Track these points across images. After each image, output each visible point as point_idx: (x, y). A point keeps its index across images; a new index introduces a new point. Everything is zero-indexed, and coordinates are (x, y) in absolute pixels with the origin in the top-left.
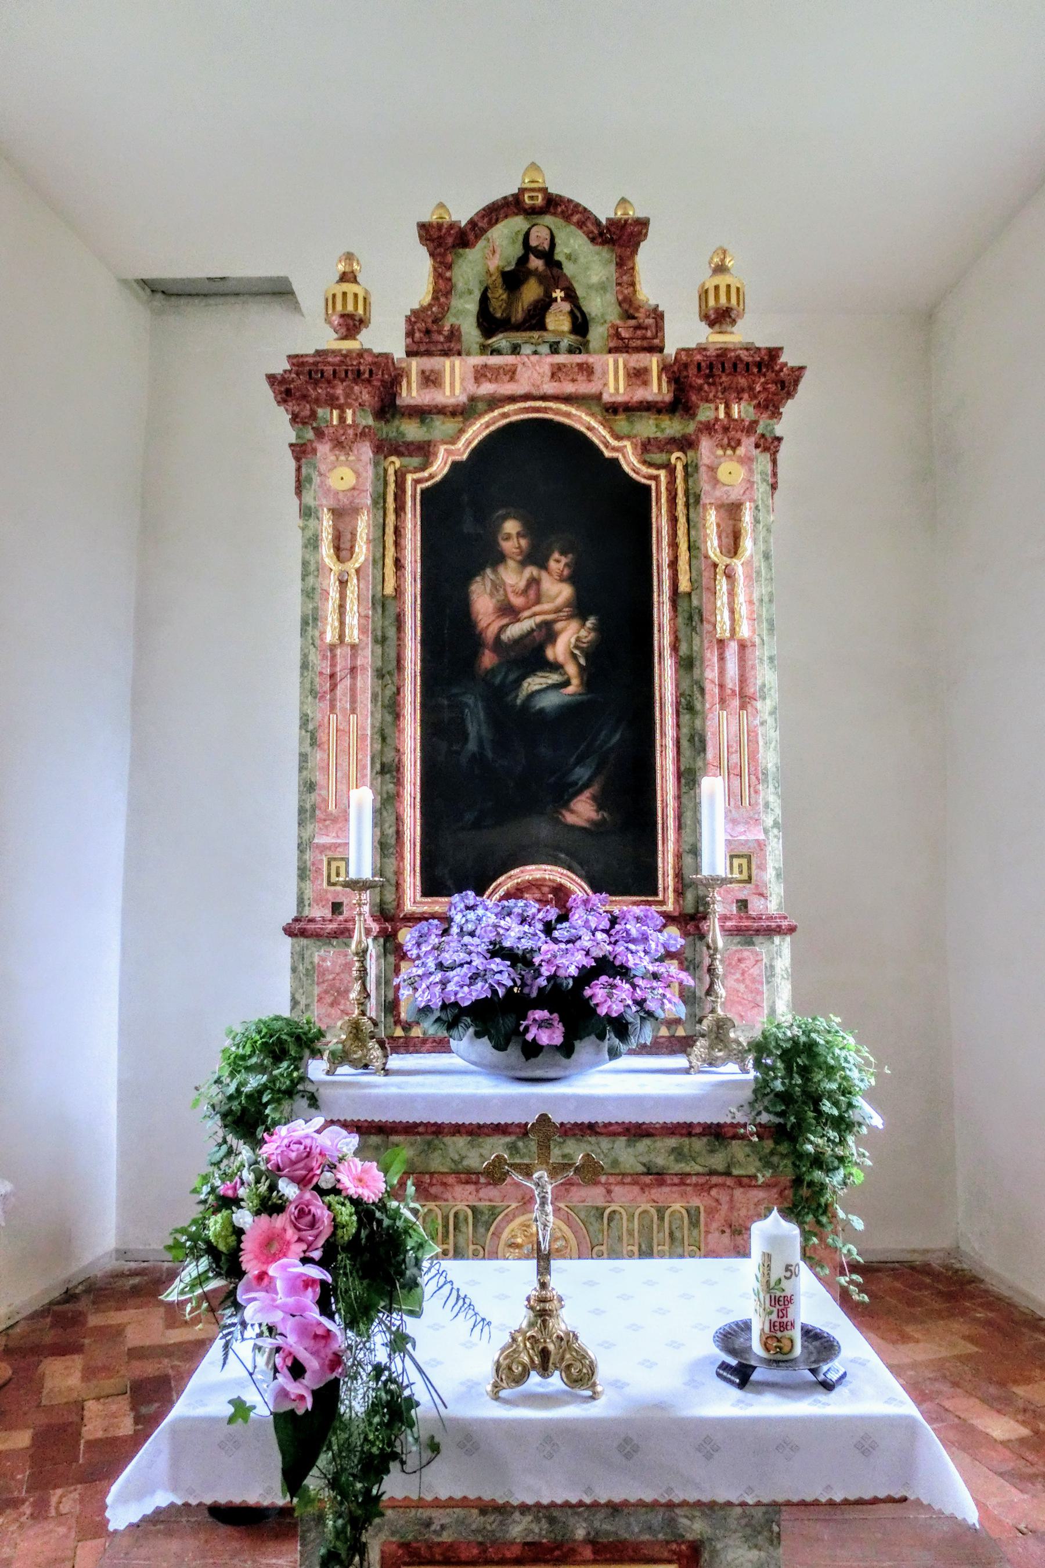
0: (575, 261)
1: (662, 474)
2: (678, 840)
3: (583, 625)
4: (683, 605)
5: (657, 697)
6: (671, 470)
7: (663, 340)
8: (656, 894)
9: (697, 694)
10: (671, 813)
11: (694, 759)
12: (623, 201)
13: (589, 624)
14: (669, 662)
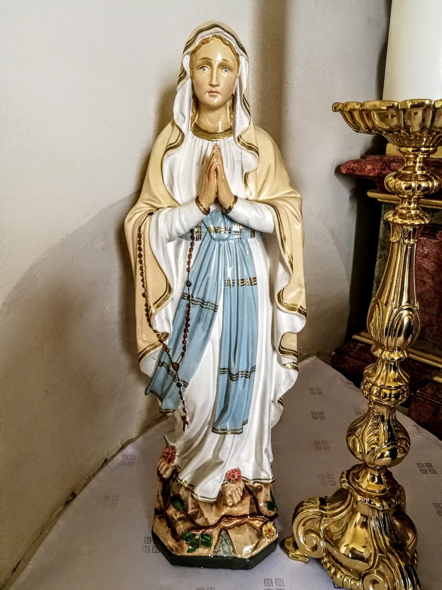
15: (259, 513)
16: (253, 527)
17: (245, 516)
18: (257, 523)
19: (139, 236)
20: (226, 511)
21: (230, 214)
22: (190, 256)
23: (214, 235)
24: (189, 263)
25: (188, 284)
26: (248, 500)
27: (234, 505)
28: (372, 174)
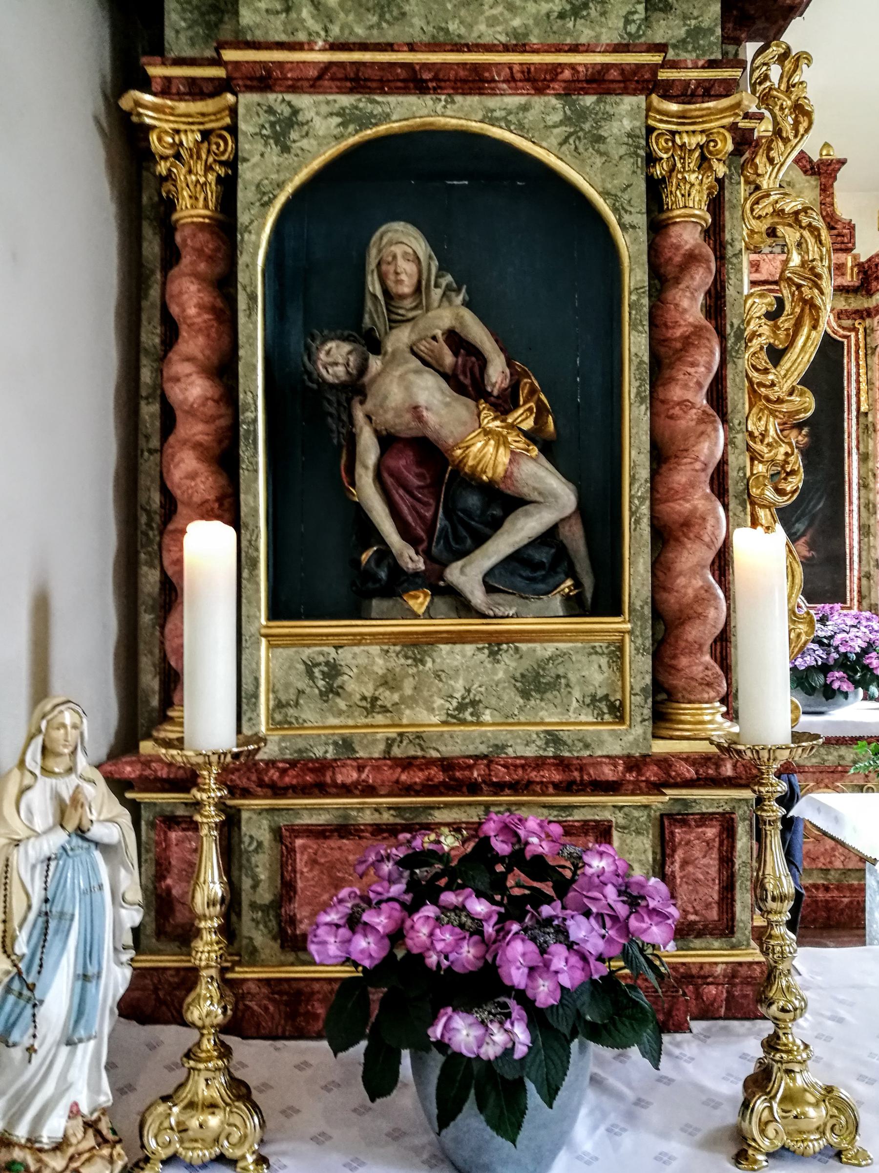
0: (793, 187)
1: (853, 335)
2: (860, 571)
3: (800, 433)
4: (861, 419)
5: (847, 479)
6: (856, 331)
7: (854, 244)
8: (845, 602)
9: (871, 477)
10: (856, 552)
11: (869, 519)
12: (826, 145)
13: (804, 432)
14: (855, 457)
15: (106, 1141)
16: (102, 1157)
17: (94, 1148)
18: (106, 1152)
19: (7, 866)
20: (71, 1151)
21: (88, 835)
22: (47, 876)
23: (70, 853)
24: (46, 882)
25: (46, 901)
26: (90, 1132)
27: (79, 1143)
28: (133, 776)
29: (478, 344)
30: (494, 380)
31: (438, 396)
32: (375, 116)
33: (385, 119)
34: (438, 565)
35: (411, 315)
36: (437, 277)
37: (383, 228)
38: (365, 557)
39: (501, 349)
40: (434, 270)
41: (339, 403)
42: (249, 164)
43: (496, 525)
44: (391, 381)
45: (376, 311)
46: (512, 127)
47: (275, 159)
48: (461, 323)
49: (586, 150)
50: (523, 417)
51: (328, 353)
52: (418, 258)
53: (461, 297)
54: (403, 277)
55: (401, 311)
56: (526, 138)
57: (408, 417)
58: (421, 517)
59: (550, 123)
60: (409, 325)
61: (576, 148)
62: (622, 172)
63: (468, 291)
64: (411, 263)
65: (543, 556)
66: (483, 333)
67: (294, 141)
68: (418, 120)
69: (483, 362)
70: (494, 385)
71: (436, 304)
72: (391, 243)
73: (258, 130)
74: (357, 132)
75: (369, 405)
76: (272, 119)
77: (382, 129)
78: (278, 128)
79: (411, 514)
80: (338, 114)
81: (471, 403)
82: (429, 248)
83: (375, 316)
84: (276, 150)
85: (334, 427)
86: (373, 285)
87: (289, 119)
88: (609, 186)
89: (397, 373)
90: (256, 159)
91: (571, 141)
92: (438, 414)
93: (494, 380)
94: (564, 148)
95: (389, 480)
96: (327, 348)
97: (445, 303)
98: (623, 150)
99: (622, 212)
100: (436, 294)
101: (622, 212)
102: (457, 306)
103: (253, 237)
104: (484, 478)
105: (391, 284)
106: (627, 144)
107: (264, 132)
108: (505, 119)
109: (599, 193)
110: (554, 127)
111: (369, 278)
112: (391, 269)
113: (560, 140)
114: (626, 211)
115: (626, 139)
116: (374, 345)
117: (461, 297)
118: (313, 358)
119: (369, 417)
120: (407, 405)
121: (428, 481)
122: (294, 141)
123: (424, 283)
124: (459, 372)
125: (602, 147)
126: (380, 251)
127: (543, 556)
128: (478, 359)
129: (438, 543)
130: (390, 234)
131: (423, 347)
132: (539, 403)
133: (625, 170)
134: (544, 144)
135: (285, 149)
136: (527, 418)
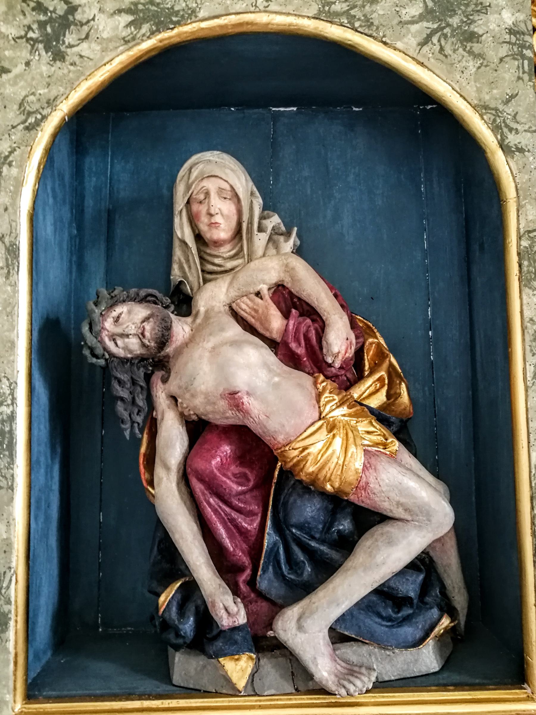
29: (315, 303)
30: (335, 350)
31: (263, 374)
32: (177, 13)
33: (190, 15)
34: (266, 608)
35: (229, 265)
36: (262, 218)
37: (194, 158)
38: (164, 599)
39: (342, 306)
40: (257, 211)
41: (134, 382)
42: (11, 75)
43: (347, 545)
44: (201, 357)
45: (188, 261)
46: (357, 24)
47: (44, 68)
48: (292, 277)
49: (455, 51)
50: (372, 389)
51: (117, 320)
52: (237, 195)
53: (291, 242)
54: (218, 219)
55: (217, 261)
56: (375, 38)
57: (222, 404)
58: (243, 533)
59: (407, 18)
60: (228, 278)
61: (442, 49)
62: (503, 78)
63: (299, 235)
64: (228, 202)
65: (410, 588)
66: (321, 289)
67: (71, 46)
68: (233, 17)
69: (321, 326)
70: (336, 356)
71: (260, 252)
72: (202, 178)
73: (23, 33)
74: (153, 33)
75: (173, 385)
76: (42, 18)
77: (188, 29)
78: (49, 30)
79: (231, 537)
80: (128, 11)
81: (306, 380)
82: (251, 183)
83: (186, 266)
84: (46, 57)
85: (125, 415)
86: (182, 228)
87: (64, 17)
88: (487, 97)
89: (209, 345)
90: (21, 67)
91: (435, 39)
92: (263, 400)
93: (335, 350)
94: (426, 49)
95: (198, 487)
96: (115, 314)
97: (272, 251)
98: (504, 50)
99: (505, 130)
100: (260, 240)
101: (505, 130)
102: (285, 254)
103: (14, 171)
104: (328, 487)
105: (203, 227)
106: (509, 43)
107: (31, 35)
108: (346, 13)
109: (474, 107)
110: (412, 22)
111: (177, 220)
112: (203, 209)
113: (420, 39)
114: (511, 130)
115: (507, 37)
116: (182, 302)
117: (291, 242)
118: (96, 328)
119: (174, 399)
120: (221, 390)
121: (251, 484)
122: (71, 46)
123: (244, 226)
124: (290, 339)
125: (476, 48)
126: (188, 187)
127: (410, 588)
128: (313, 321)
129: (264, 571)
130: (201, 166)
131: (245, 307)
132: (391, 370)
133: (507, 76)
134: (399, 45)
135: (59, 56)
136: (377, 391)
